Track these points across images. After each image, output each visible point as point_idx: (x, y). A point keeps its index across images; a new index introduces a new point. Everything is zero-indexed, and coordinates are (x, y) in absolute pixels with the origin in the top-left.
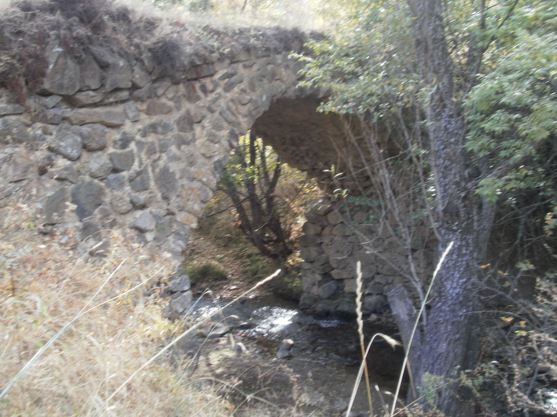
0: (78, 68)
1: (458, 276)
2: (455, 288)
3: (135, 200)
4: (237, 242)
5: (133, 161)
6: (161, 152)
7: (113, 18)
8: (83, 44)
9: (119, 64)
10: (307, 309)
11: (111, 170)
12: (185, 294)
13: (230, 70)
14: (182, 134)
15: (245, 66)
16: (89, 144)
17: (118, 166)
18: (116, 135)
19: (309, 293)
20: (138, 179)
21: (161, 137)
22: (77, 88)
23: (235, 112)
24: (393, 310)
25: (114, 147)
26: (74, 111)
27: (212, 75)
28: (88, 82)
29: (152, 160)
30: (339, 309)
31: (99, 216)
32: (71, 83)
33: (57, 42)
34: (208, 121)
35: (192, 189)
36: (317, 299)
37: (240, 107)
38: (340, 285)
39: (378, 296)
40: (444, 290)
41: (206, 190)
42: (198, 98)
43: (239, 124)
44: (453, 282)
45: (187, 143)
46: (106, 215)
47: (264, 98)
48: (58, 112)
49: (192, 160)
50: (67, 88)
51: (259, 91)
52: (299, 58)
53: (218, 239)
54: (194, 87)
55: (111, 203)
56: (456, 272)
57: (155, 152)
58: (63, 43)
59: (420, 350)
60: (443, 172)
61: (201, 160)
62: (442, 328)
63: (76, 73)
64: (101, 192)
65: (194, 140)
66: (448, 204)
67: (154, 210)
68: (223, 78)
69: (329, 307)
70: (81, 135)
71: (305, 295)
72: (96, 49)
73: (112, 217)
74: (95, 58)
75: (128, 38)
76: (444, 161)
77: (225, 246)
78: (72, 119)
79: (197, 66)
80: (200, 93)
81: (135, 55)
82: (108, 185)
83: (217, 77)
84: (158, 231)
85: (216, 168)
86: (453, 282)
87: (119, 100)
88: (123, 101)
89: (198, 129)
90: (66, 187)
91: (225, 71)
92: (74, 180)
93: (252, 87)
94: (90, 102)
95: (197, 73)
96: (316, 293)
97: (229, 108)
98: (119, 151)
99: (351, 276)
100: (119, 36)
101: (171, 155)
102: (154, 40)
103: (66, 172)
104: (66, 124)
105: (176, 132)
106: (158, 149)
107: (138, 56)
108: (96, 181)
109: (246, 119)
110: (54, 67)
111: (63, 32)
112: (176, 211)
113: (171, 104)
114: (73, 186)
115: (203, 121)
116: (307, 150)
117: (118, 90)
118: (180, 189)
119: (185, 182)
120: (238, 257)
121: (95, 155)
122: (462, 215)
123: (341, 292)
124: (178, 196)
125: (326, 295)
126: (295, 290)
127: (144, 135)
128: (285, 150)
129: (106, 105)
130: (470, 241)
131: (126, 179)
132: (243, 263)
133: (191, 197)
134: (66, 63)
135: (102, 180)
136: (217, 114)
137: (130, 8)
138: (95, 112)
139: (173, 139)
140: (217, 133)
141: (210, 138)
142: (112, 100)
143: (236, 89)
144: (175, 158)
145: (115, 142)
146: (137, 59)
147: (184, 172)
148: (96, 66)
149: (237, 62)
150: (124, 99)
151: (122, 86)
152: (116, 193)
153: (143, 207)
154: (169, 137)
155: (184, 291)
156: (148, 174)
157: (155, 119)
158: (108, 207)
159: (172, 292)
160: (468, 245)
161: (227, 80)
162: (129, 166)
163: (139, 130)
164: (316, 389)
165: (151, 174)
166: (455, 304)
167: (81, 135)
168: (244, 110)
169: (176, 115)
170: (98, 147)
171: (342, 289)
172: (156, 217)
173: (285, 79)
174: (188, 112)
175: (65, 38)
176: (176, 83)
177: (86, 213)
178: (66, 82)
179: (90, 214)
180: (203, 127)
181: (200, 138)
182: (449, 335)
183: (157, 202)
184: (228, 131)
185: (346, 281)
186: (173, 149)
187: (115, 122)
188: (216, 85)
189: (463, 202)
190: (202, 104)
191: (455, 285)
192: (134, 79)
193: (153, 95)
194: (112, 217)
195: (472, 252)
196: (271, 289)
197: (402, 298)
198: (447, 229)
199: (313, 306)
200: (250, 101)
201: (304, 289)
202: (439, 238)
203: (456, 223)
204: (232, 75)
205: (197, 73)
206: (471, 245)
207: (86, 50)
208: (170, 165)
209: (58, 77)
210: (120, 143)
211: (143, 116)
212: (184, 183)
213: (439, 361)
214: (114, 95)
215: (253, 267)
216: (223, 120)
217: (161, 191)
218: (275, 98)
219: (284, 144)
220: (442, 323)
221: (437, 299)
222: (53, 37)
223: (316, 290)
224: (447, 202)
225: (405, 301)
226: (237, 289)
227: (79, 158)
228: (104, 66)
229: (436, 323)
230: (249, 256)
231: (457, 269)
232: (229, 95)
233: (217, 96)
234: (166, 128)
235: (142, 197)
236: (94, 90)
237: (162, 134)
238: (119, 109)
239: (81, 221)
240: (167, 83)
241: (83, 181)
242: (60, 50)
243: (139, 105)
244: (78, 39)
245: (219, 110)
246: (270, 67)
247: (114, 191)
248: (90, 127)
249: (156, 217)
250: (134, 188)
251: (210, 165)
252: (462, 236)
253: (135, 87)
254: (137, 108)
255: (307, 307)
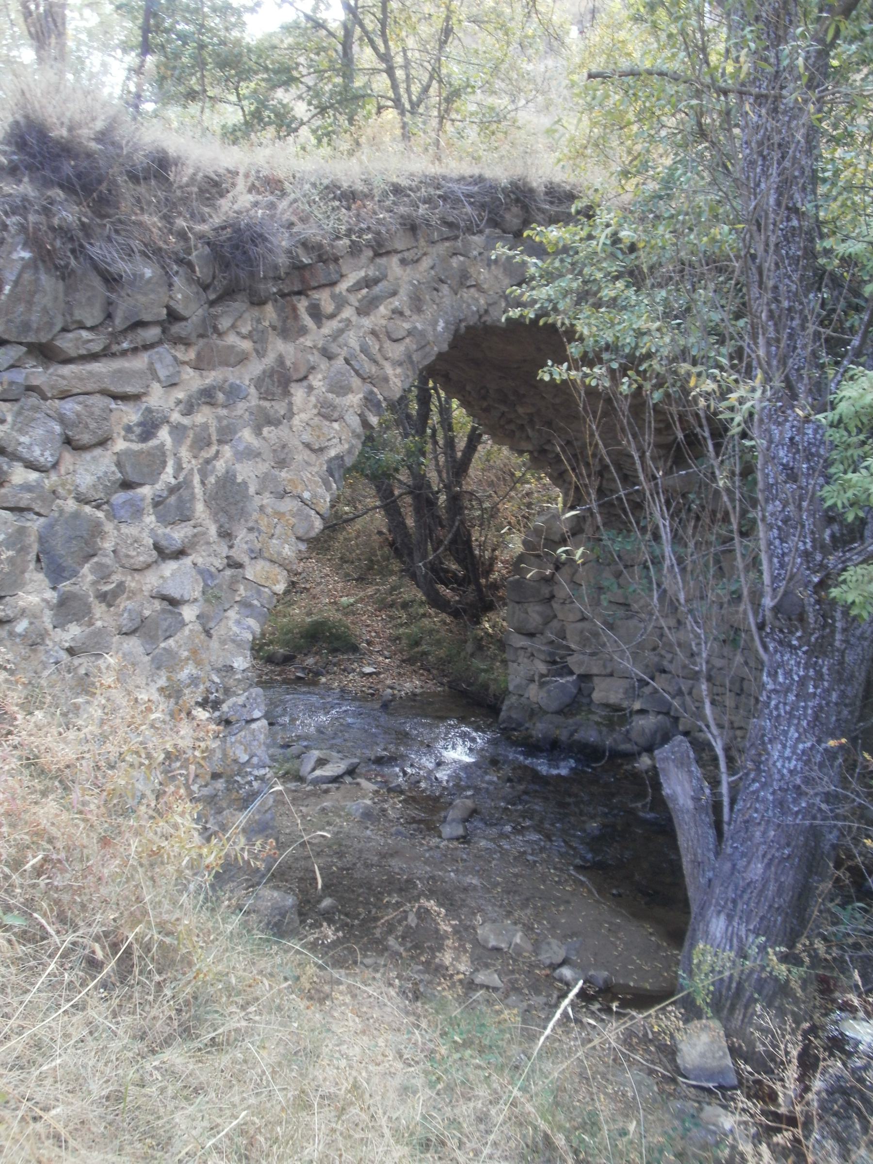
0: (61, 285)
1: (796, 735)
2: (789, 759)
3: (164, 543)
4: (385, 572)
5: (164, 463)
6: (220, 442)
7: (134, 178)
8: (71, 239)
9: (142, 276)
10: (514, 729)
11: (117, 485)
12: (254, 726)
13: (372, 272)
14: (266, 404)
15: (403, 262)
16: (77, 437)
17: (133, 477)
18: (131, 415)
19: (522, 696)
20: (173, 499)
21: (223, 412)
22: (58, 327)
23: (379, 357)
24: (665, 785)
25: (125, 439)
26: (51, 370)
27: (333, 284)
28: (78, 314)
29: (201, 461)
30: (576, 736)
31: (91, 578)
32: (45, 319)
33: (21, 238)
34: (320, 376)
35: (280, 515)
36: (534, 712)
37: (388, 344)
38: (583, 685)
39: (660, 717)
40: (767, 760)
41: (308, 516)
42: (303, 331)
43: (386, 379)
44: (784, 746)
45: (273, 422)
46: (104, 575)
47: (440, 328)
48: (19, 377)
49: (283, 456)
50: (38, 330)
51: (430, 311)
52: (514, 257)
53: (346, 562)
54: (295, 309)
55: (114, 551)
56: (792, 729)
57: (209, 444)
58: (33, 241)
59: (714, 869)
60: (779, 528)
61: (302, 455)
62: (758, 834)
63: (56, 299)
64: (96, 530)
65: (290, 414)
66: (786, 593)
67: (200, 561)
68: (356, 288)
69: (558, 732)
70: (62, 419)
71: (513, 699)
72: (97, 250)
73: (116, 578)
74: (95, 267)
75: (167, 218)
76: (784, 507)
77: (360, 579)
78: (45, 388)
79: (305, 267)
80: (307, 321)
81: (176, 253)
82: (111, 516)
83: (343, 286)
84: (207, 601)
85: (330, 472)
86: (784, 746)
87: (140, 343)
88: (146, 347)
89: (298, 393)
90: (29, 524)
91: (362, 273)
92: (42, 511)
93: (417, 302)
94: (83, 352)
95: (303, 281)
96: (535, 700)
97: (364, 350)
98: (136, 447)
99: (608, 671)
100: (145, 218)
101: (241, 448)
102: (217, 221)
103: (28, 496)
104: (33, 400)
105: (254, 400)
106: (214, 438)
107: (182, 255)
108: (87, 509)
109: (399, 370)
110: (11, 291)
111: (32, 218)
112: (245, 559)
113: (246, 345)
114: (42, 520)
115: (311, 377)
116: (531, 416)
117: (141, 324)
118: (255, 515)
119: (267, 499)
120: (384, 605)
121: (87, 456)
122: (811, 620)
123: (585, 701)
124: (251, 530)
125: (554, 706)
126: (493, 687)
127: (189, 409)
128: (486, 410)
129: (114, 355)
130: (825, 670)
131: (149, 500)
132: (392, 618)
133: (278, 530)
134: (38, 279)
135: (98, 507)
136: (340, 362)
137: (172, 152)
138: (90, 372)
139: (247, 416)
140: (337, 401)
141: (323, 410)
142: (125, 345)
143: (382, 310)
144: (250, 454)
145: (129, 429)
146: (180, 261)
147: (265, 481)
148: (97, 282)
149: (388, 253)
150: (153, 341)
151: (147, 318)
152: (125, 529)
153: (180, 554)
154: (239, 412)
155: (254, 720)
156: (193, 488)
157: (212, 377)
158: (107, 561)
159: (228, 723)
160: (820, 676)
161: (365, 291)
162: (153, 477)
163: (179, 402)
164: (509, 914)
165: (198, 490)
166: (786, 790)
167: (62, 419)
168: (396, 351)
169: (256, 368)
170: (94, 440)
171: (589, 695)
172: (205, 574)
173: (485, 286)
174: (281, 360)
175: (37, 230)
176: (259, 303)
177: (66, 574)
178: (35, 318)
179: (75, 574)
180: (311, 388)
181: (303, 410)
182: (770, 847)
183: (208, 543)
184: (361, 396)
185: (596, 680)
186: (247, 435)
187: (129, 389)
188: (341, 303)
189: (815, 593)
190: (309, 343)
191: (788, 752)
192: (172, 303)
193: (210, 330)
194: (116, 578)
195: (828, 691)
196: (445, 680)
197: (681, 763)
198: (781, 642)
199: (527, 725)
200: (410, 333)
201: (511, 688)
202: (765, 657)
203: (799, 634)
204: (376, 281)
205: (303, 281)
206: (826, 677)
207: (78, 251)
208: (238, 467)
209: (21, 308)
210: (138, 430)
211: (188, 373)
212: (265, 502)
213: (746, 897)
214: (130, 336)
215: (414, 629)
216: (353, 373)
217: (216, 521)
218: (463, 324)
219: (484, 398)
220: (759, 824)
221: (752, 776)
222: (13, 230)
223: (534, 693)
224: (781, 591)
225: (690, 772)
226: (377, 674)
227: (55, 465)
228: (111, 280)
229: (746, 822)
230: (405, 606)
231: (796, 721)
232: (367, 322)
233: (341, 325)
234: (234, 393)
235: (178, 535)
236: (91, 329)
237: (225, 406)
238: (139, 362)
239: (54, 589)
240: (239, 305)
241: (61, 511)
242: (26, 255)
243: (181, 353)
244: (63, 232)
245: (344, 352)
246: (455, 262)
247: (123, 526)
248: (80, 403)
249: (205, 574)
250: (162, 519)
251: (320, 465)
252: (809, 658)
253: (174, 316)
254: (175, 358)
255: (514, 726)
